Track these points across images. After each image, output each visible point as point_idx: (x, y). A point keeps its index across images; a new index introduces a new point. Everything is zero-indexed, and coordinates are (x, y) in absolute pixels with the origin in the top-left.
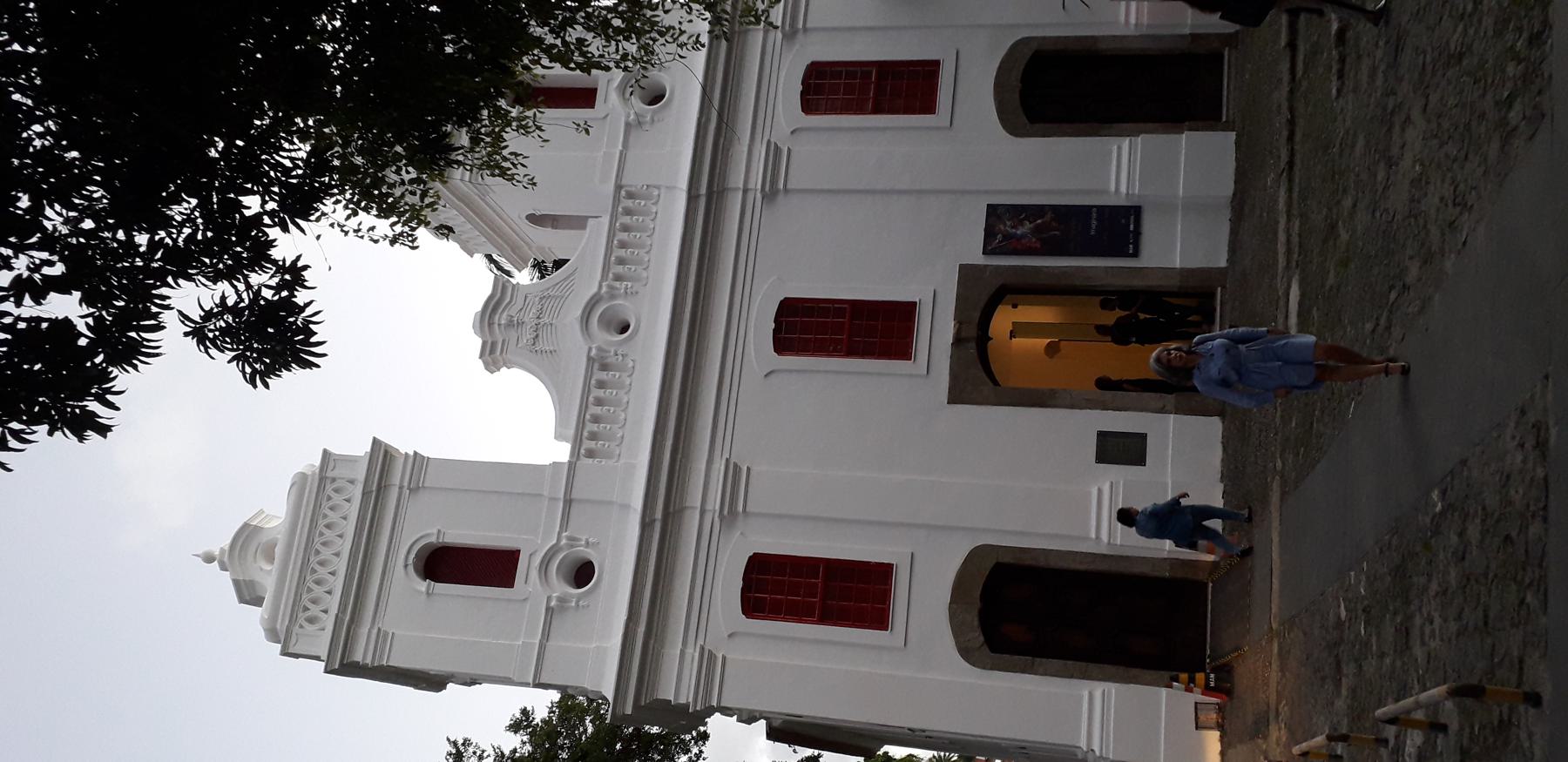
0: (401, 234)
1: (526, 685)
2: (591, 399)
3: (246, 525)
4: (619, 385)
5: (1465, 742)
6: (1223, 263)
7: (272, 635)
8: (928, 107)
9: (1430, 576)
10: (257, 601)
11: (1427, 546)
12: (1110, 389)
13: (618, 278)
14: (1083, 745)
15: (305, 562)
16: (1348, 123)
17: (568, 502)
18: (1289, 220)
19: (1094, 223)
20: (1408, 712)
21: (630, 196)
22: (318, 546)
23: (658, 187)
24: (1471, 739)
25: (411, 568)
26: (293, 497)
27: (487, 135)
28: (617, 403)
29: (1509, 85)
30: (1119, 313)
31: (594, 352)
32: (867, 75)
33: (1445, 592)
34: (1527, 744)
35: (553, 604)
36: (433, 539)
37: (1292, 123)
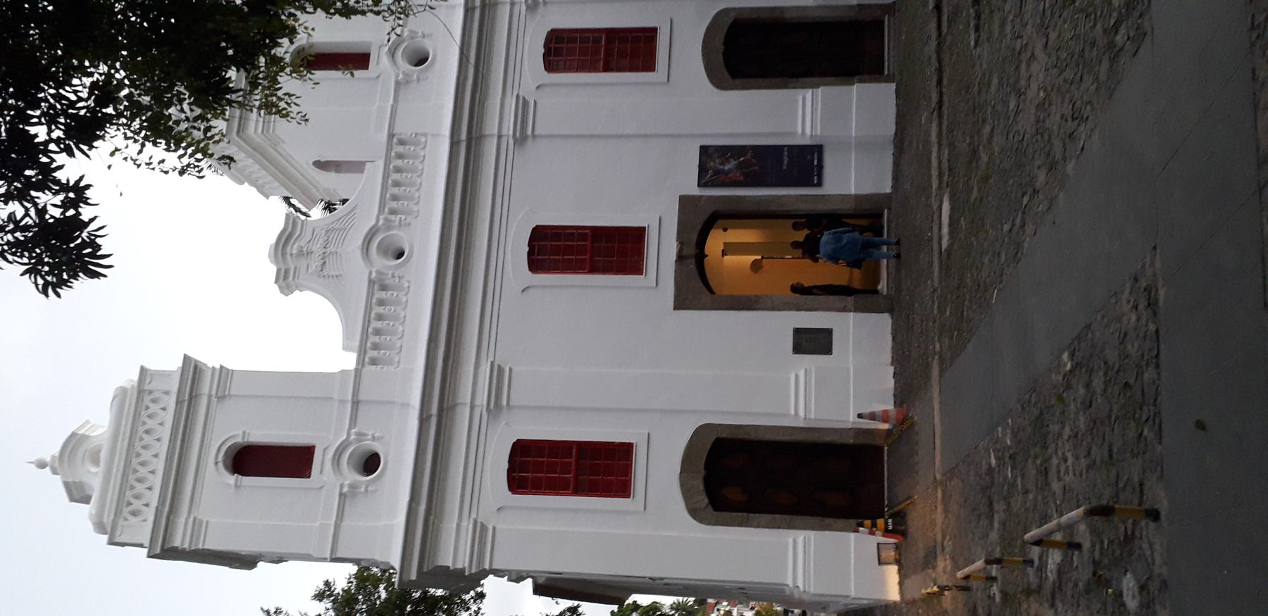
0: (188, 166)
1: (324, 560)
2: (373, 315)
3: (73, 435)
4: (396, 303)
5: (1097, 555)
6: (888, 190)
7: (100, 527)
8: (649, 66)
9: (1063, 423)
10: (86, 500)
11: (1060, 398)
12: (804, 294)
13: (393, 212)
14: (790, 583)
15: (128, 463)
16: (985, 66)
17: (356, 403)
18: (939, 149)
19: (786, 160)
20: (1051, 533)
21: (402, 142)
22: (138, 449)
23: (425, 135)
24: (1101, 553)
25: (221, 465)
26: (115, 406)
27: (264, 79)
28: (396, 318)
29: (1115, 15)
30: (806, 232)
31: (374, 275)
32: (597, 41)
33: (1076, 436)
34: (1148, 553)
35: (345, 489)
36: (239, 440)
37: (940, 71)
